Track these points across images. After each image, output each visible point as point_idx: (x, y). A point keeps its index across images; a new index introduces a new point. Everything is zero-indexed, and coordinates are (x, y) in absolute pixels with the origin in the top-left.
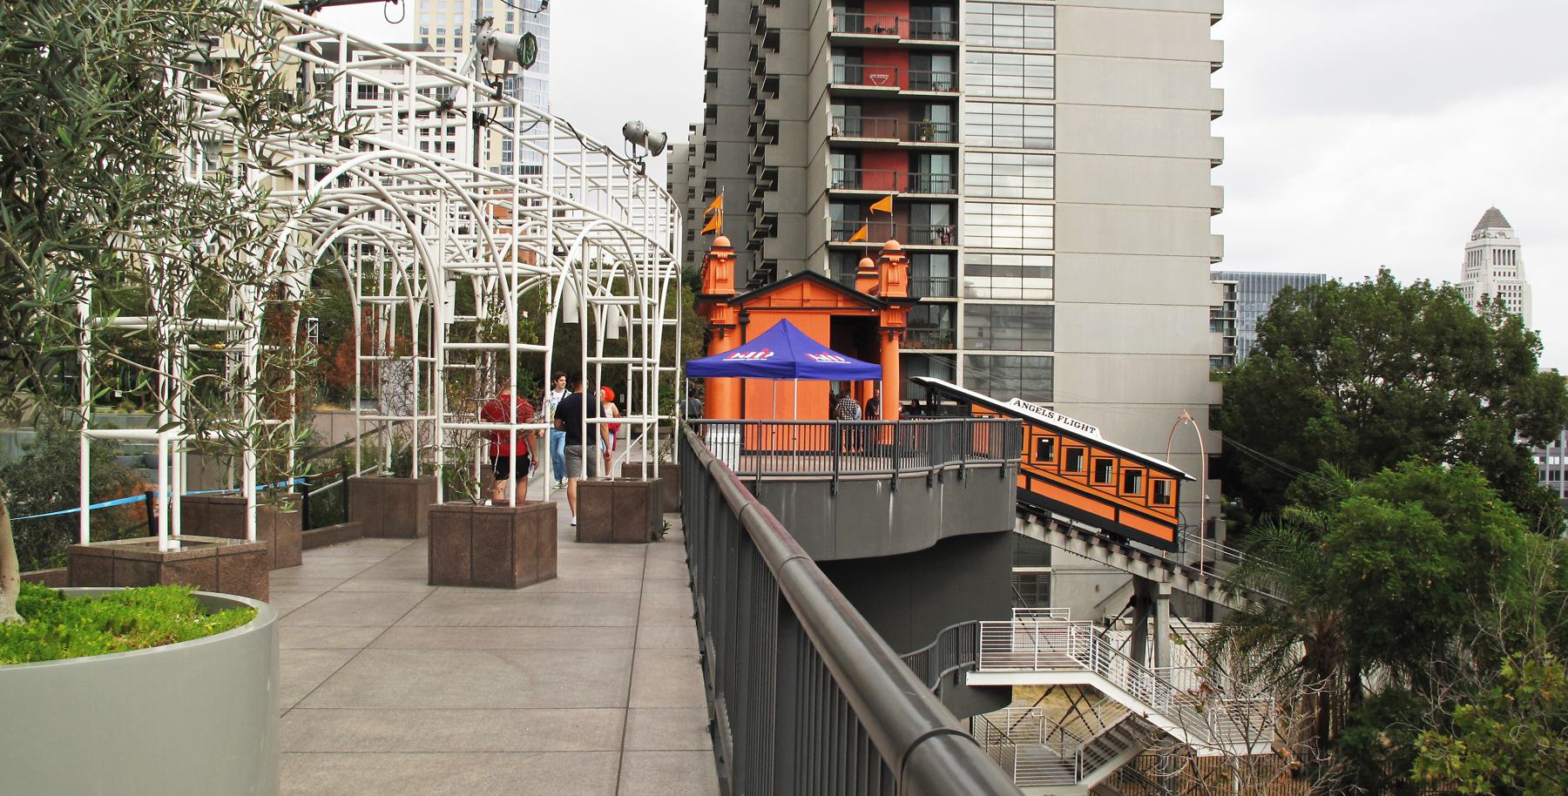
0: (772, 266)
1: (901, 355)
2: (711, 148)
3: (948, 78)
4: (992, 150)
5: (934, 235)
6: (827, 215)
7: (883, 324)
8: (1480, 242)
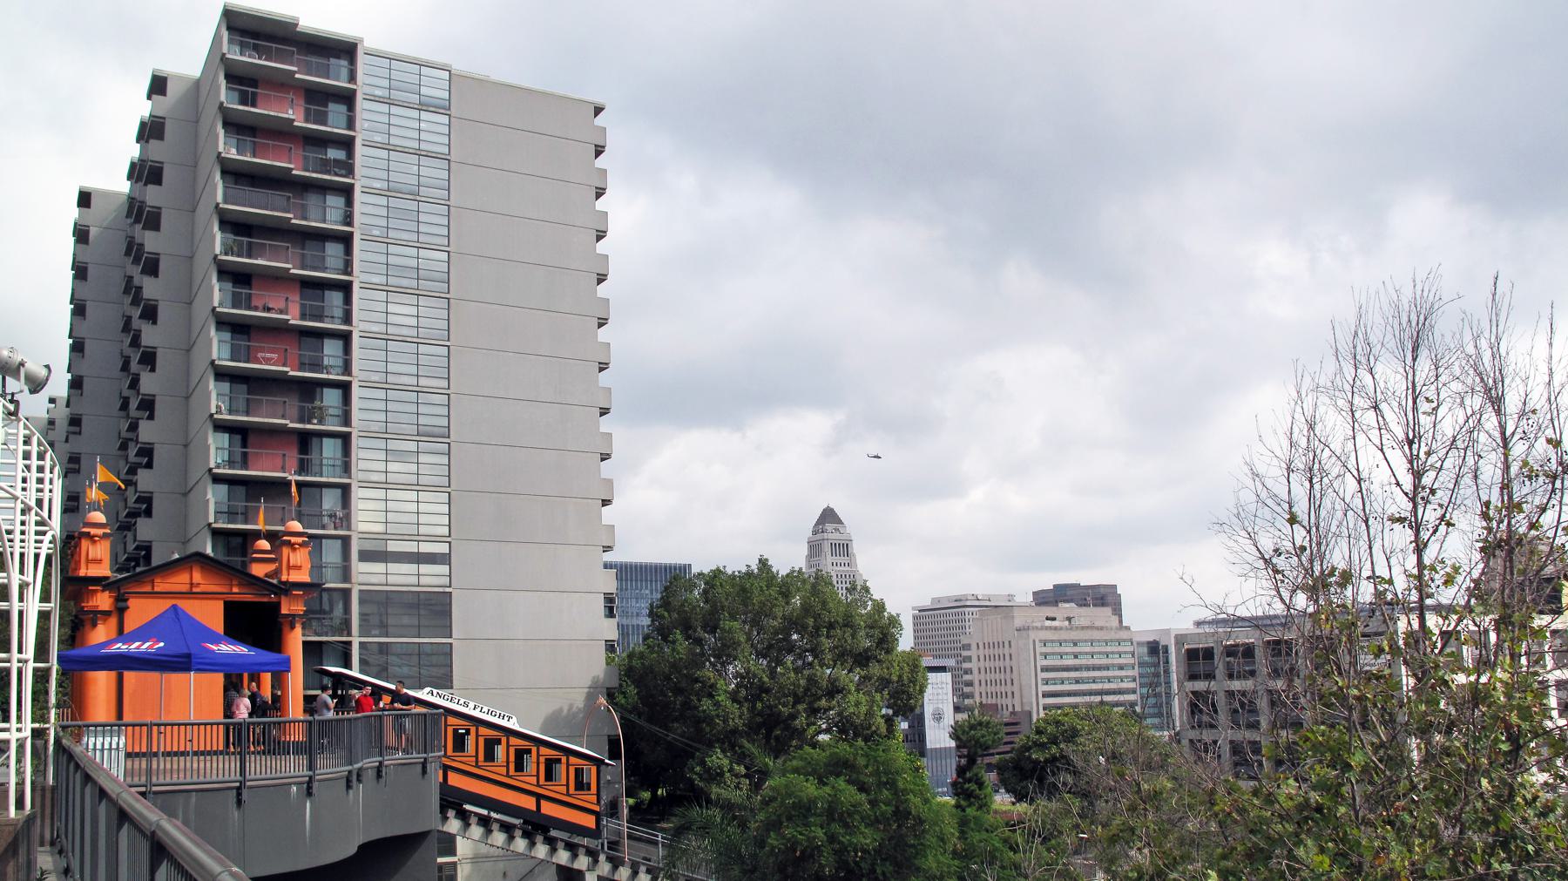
0: (147, 548)
1: (305, 643)
2: (75, 421)
3: (340, 362)
4: (385, 435)
5: (326, 520)
6: (210, 496)
7: (284, 611)
8: (819, 536)
